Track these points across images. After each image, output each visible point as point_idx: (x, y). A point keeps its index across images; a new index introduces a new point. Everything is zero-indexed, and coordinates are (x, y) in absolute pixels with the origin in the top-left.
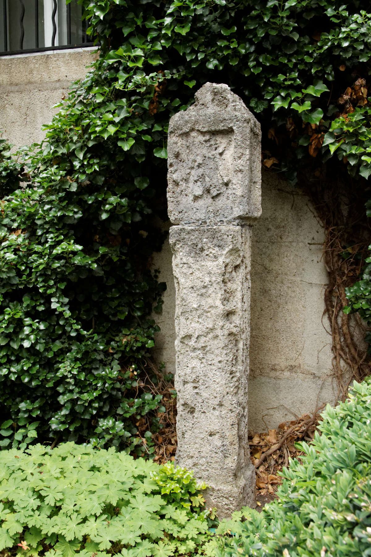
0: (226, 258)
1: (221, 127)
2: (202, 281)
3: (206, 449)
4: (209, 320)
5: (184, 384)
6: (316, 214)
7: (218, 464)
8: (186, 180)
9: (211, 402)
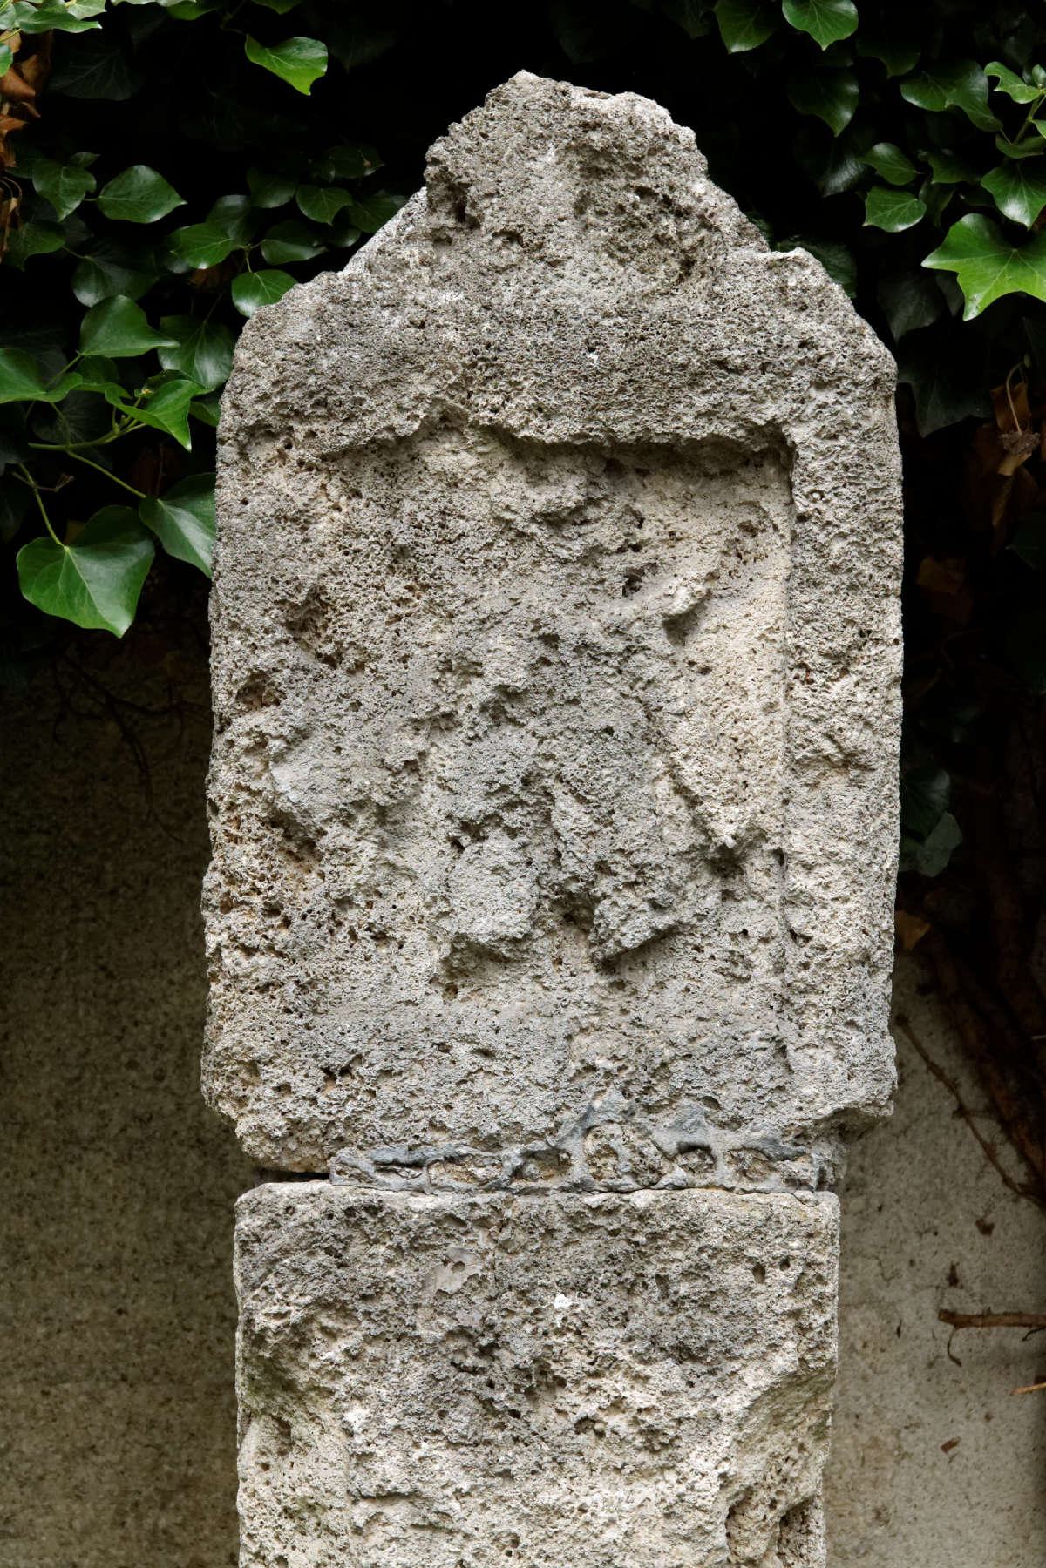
6: (971, 1095)
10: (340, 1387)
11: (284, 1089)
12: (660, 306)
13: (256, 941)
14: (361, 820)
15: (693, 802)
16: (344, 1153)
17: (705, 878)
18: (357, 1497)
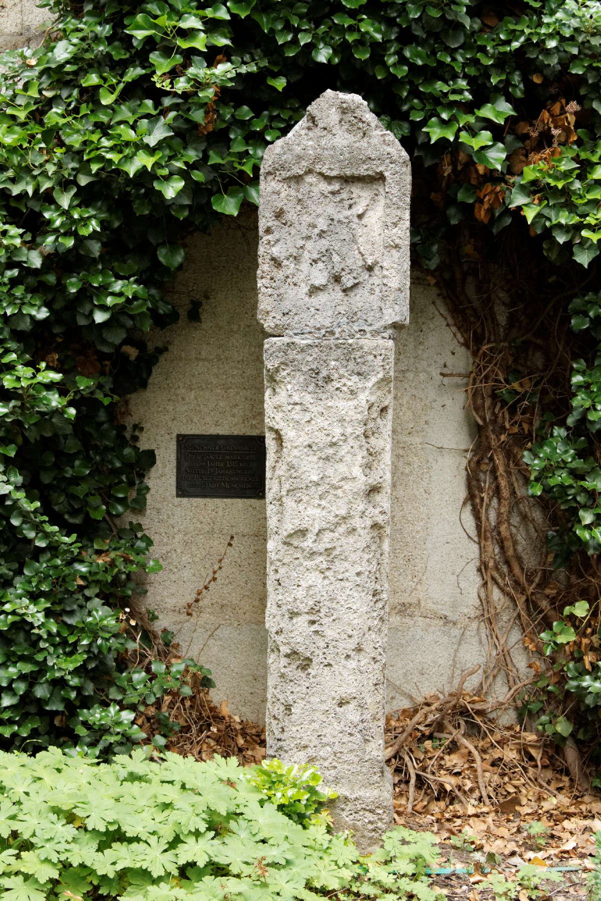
0: (371, 394)
1: (362, 171)
2: (328, 435)
3: (332, 730)
4: (340, 502)
5: (291, 618)
7: (355, 753)
9: (341, 645)
10: (286, 381)
12: (358, 144)
14: (291, 259)
15: (363, 255)
17: (366, 272)
18: (289, 404)
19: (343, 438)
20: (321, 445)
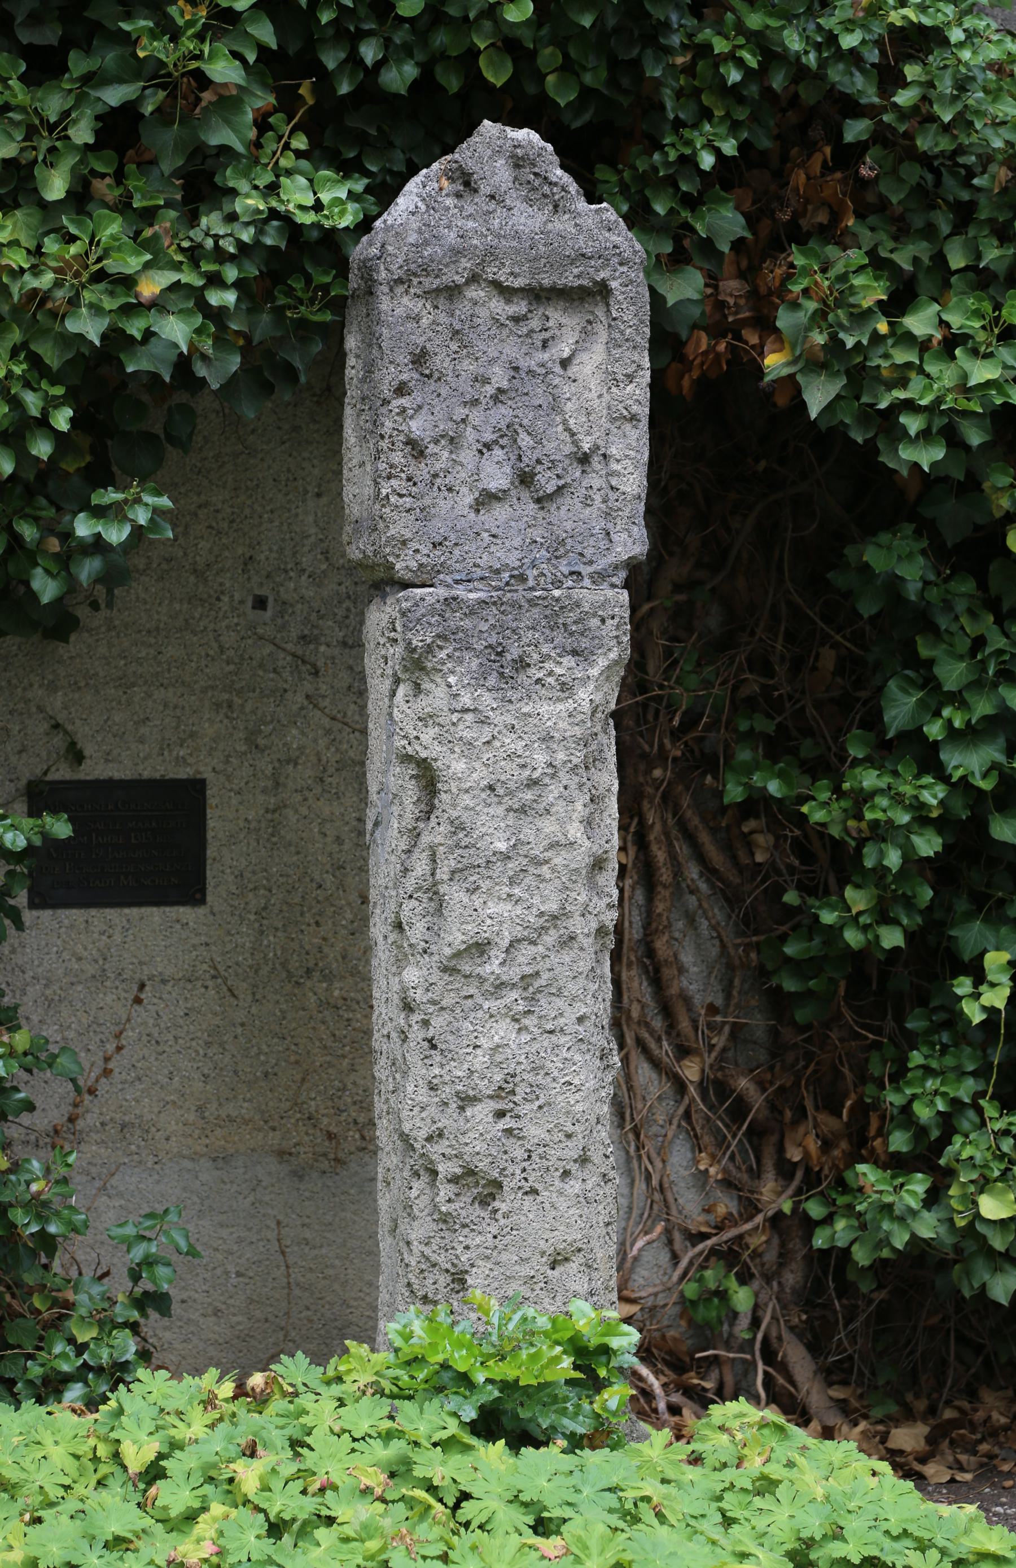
1: (570, 278)
4: (547, 889)
5: (462, 1109)
8: (454, 442)
9: (553, 1153)
11: (417, 551)
13: (404, 492)
14: (443, 442)
16: (441, 576)
18: (453, 711)
19: (550, 771)
20: (512, 785)
